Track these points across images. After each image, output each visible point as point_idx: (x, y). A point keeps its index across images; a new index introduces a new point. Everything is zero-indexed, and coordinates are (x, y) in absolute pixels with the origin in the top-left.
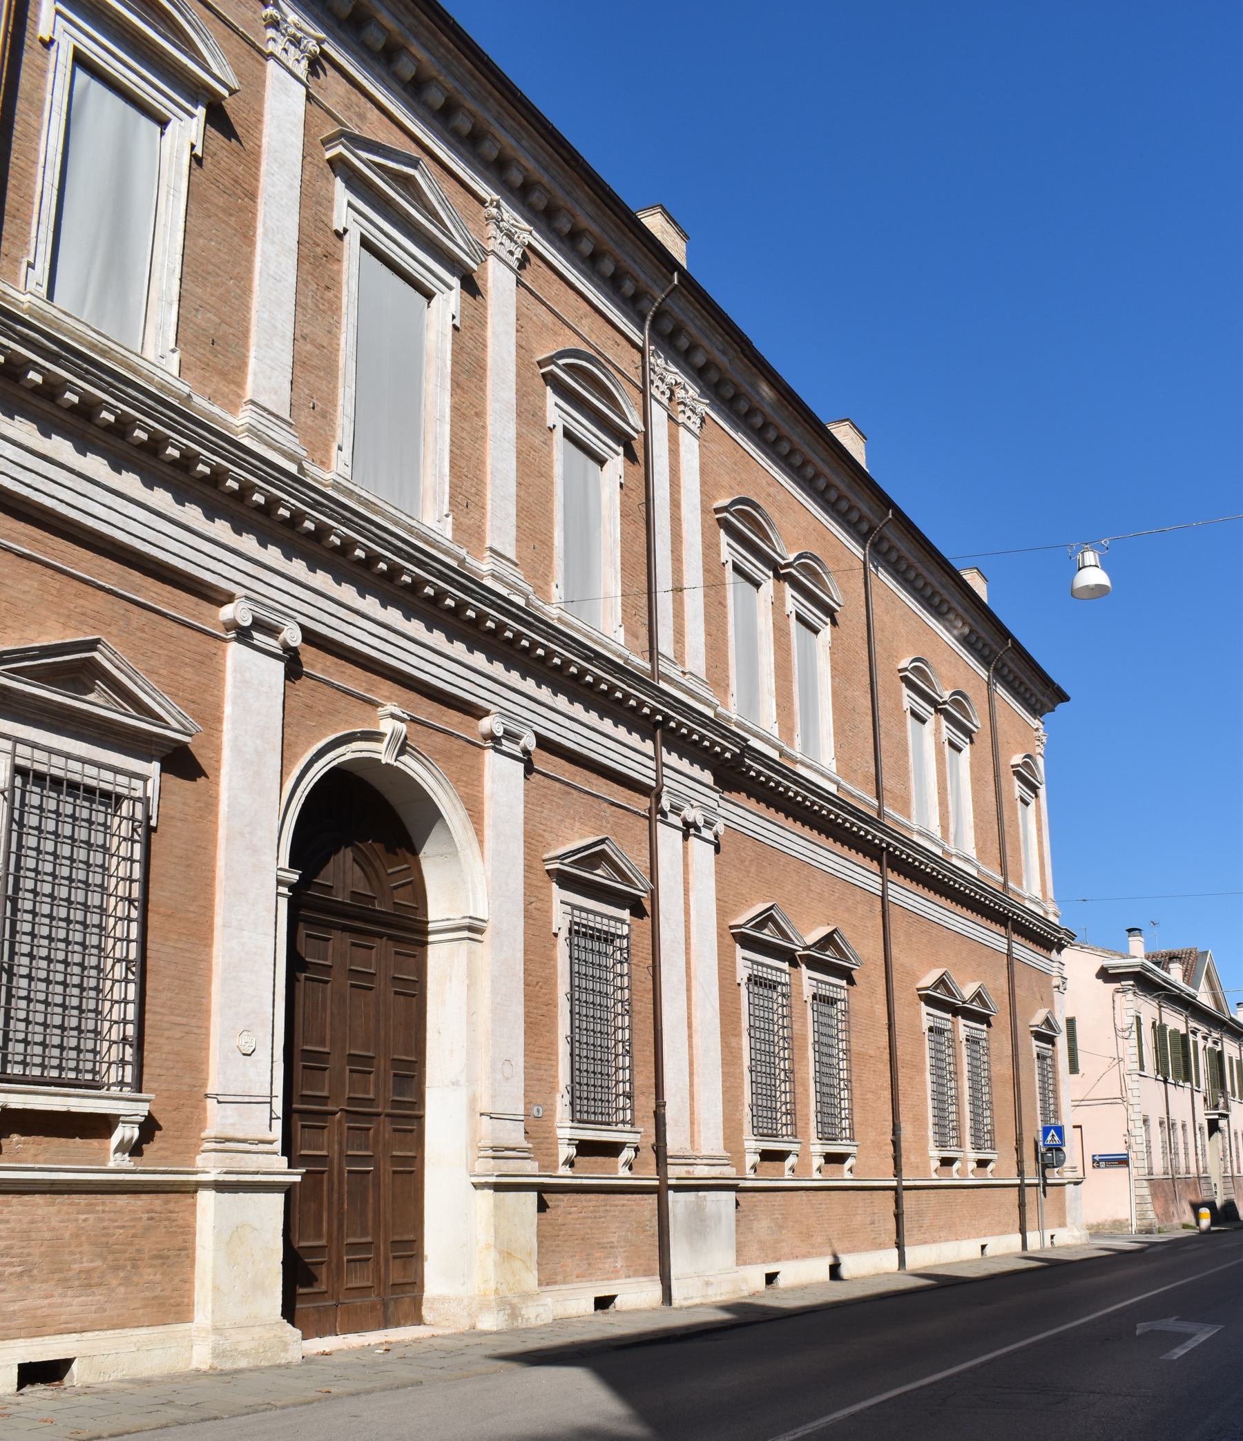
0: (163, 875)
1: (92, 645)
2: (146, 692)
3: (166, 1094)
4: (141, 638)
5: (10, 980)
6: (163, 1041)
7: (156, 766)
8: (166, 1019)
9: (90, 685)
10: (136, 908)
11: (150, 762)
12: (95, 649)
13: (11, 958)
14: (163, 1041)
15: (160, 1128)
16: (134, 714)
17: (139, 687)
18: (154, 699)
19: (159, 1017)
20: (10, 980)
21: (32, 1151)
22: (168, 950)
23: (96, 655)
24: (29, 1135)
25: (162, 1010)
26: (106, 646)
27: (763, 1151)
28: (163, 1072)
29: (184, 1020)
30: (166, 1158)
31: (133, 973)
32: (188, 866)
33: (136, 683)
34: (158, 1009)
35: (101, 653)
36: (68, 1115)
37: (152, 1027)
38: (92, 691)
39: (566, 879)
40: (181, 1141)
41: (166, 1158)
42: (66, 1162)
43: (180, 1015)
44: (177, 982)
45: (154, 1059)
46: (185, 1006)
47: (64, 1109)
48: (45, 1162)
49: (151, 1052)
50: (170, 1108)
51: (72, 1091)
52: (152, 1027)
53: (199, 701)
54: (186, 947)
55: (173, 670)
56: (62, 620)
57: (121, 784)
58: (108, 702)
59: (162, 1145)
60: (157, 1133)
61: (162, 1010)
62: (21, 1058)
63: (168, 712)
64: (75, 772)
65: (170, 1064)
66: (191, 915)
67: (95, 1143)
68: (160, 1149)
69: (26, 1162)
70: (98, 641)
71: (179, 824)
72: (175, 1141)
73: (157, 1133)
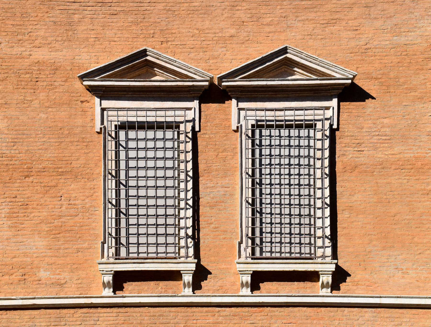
1: (284, 51)
5: (261, 215)
7: (334, 102)
12: (287, 53)
15: (350, 275)
23: (288, 55)
27: (254, 272)
35: (150, 56)
39: (242, 91)
57: (309, 116)
70: (145, 51)
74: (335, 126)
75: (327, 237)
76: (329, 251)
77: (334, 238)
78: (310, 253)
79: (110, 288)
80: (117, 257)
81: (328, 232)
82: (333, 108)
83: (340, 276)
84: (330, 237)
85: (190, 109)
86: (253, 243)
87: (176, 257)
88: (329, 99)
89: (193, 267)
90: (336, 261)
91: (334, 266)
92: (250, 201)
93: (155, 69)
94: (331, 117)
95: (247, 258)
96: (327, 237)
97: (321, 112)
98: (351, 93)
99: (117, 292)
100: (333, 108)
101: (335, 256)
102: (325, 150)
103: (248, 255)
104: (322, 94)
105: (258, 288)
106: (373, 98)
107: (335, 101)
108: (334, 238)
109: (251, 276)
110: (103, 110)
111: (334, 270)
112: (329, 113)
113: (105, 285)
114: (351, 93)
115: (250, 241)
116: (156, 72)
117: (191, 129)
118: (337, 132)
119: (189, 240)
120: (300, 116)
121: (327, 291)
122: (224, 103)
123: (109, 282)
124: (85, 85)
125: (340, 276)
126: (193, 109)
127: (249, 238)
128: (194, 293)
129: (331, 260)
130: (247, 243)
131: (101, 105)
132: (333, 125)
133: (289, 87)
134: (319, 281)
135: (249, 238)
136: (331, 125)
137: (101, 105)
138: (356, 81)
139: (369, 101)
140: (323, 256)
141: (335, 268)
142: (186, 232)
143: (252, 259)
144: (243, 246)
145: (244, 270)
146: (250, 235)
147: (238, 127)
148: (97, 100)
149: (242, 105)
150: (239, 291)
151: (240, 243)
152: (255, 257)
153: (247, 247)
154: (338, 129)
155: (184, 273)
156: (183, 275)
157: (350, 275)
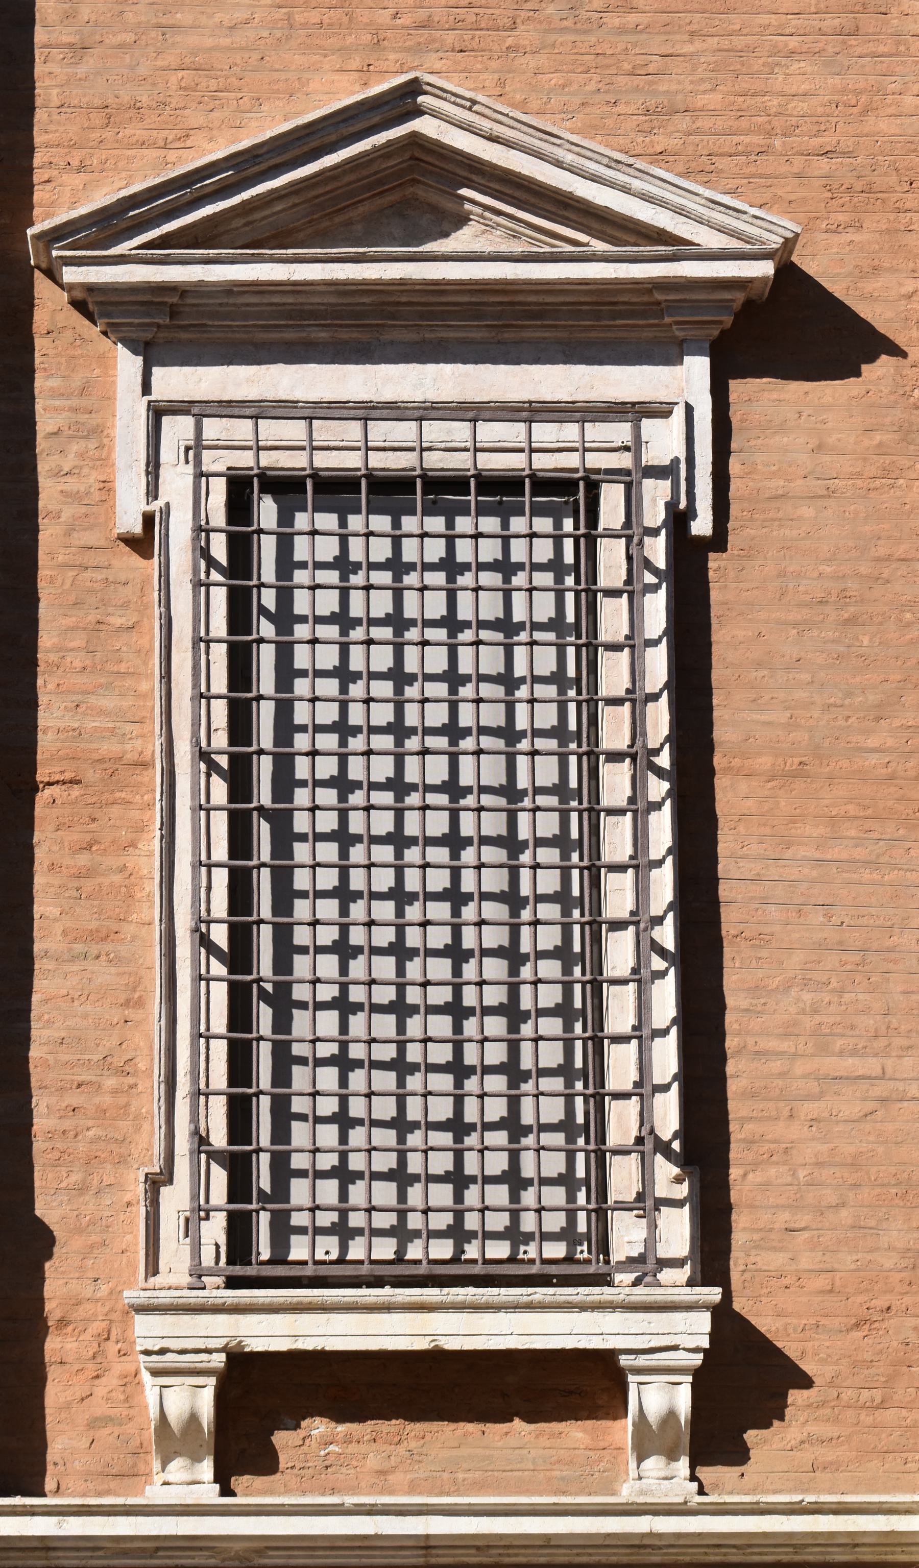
0: (759, 665)
1: (404, 101)
2: (594, 178)
3: (822, 1282)
4: (622, 31)
5: (282, 1023)
6: (795, 1131)
7: (693, 375)
8: (800, 1068)
9: (448, 205)
10: (660, 772)
11: (674, 359)
12: (418, 112)
13: (283, 963)
14: (795, 1131)
15: (806, 1382)
16: (599, 246)
17: (571, 169)
18: (626, 190)
19: (776, 1066)
20: (282, 1023)
21: (373, 1462)
22: (793, 873)
23: (425, 126)
24: (359, 1417)
25: (786, 1046)
26: (442, 93)
28: (803, 1220)
29: (872, 1065)
30: (833, 1466)
31: (662, 952)
32: (852, 621)
33: (559, 164)
34: (772, 1044)
36: (436, 1360)
37: (751, 1095)
38: (462, 220)
40: (889, 1415)
41: (833, 1466)
42: (479, 1487)
43: (854, 1053)
44: (832, 960)
45: (766, 1185)
46: (869, 1022)
47: (421, 1344)
48: (412, 1489)
49: (755, 1166)
50: (836, 1323)
51: (432, 1294)
52: (751, 1095)
53: (847, 143)
54: (860, 853)
55: (744, 84)
56: (355, 63)
57: (556, 448)
58: (516, 236)
59: (812, 1428)
60: (795, 1396)
61: (786, 1046)
62: (334, 1217)
63: (680, 211)
64: (393, 448)
65: (830, 1196)
66: (874, 759)
67: (575, 1433)
68: (808, 1440)
69: (354, 1490)
70: (413, 88)
71: (807, 511)
72: (866, 1418)
73: (795, 1396)
74: (702, 526)
75: (663, 1148)
76: (676, 1232)
77: (704, 1146)
78: (568, 1234)
79: (196, 1459)
80: (238, 1270)
81: (668, 1115)
82: (689, 409)
83: (743, 1385)
84: (676, 1146)
85: (662, 411)
86: (240, 1187)
87: (584, 1269)
88: (669, 353)
89: (696, 1329)
90: (714, 1294)
91: (703, 1322)
92: (220, 935)
93: (465, 192)
94: (676, 461)
95: (198, 1273)
96: (663, 1148)
97: (620, 432)
98: (786, 328)
99: (239, 1482)
100: (689, 409)
101: (712, 1256)
102: (650, 651)
103: (208, 1258)
104: (527, 334)
105: (265, 1463)
106: (896, 351)
107: (697, 368)
108: (704, 1146)
109: (694, 1385)
110: (158, 413)
111: (706, 1344)
112: (664, 441)
113: (171, 1441)
114: (786, 328)
115: (219, 1177)
116: (468, 206)
117: (662, 516)
118: (715, 561)
119: (665, 1170)
120: (502, 448)
121: (666, 1478)
122: (858, 374)
123: (671, 1415)
124: (69, 288)
125: (743, 1385)
126: (679, 413)
127: (214, 1155)
128: (226, 1491)
129: (690, 1283)
130: (200, 1184)
131: (146, 388)
132: (690, 513)
133: (443, 292)
134: (626, 1416)
135: (214, 1155)
136: (679, 519)
137: (146, 388)
138: (810, 263)
139: (881, 369)
140: (647, 1265)
141: (712, 1335)
142: (644, 1116)
143: (233, 1283)
144: (175, 1200)
145: (655, 1342)
146: (219, 1139)
147: (148, 520)
148: (127, 364)
149: (173, 382)
150: (147, 1476)
151: (156, 1183)
152: (251, 1271)
153: (200, 1212)
154: (719, 540)
155: (639, 1371)
156: (631, 1378)
157: (806, 1382)
